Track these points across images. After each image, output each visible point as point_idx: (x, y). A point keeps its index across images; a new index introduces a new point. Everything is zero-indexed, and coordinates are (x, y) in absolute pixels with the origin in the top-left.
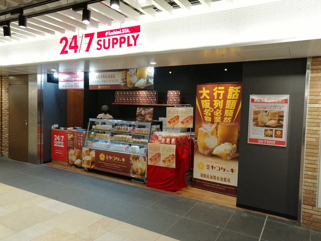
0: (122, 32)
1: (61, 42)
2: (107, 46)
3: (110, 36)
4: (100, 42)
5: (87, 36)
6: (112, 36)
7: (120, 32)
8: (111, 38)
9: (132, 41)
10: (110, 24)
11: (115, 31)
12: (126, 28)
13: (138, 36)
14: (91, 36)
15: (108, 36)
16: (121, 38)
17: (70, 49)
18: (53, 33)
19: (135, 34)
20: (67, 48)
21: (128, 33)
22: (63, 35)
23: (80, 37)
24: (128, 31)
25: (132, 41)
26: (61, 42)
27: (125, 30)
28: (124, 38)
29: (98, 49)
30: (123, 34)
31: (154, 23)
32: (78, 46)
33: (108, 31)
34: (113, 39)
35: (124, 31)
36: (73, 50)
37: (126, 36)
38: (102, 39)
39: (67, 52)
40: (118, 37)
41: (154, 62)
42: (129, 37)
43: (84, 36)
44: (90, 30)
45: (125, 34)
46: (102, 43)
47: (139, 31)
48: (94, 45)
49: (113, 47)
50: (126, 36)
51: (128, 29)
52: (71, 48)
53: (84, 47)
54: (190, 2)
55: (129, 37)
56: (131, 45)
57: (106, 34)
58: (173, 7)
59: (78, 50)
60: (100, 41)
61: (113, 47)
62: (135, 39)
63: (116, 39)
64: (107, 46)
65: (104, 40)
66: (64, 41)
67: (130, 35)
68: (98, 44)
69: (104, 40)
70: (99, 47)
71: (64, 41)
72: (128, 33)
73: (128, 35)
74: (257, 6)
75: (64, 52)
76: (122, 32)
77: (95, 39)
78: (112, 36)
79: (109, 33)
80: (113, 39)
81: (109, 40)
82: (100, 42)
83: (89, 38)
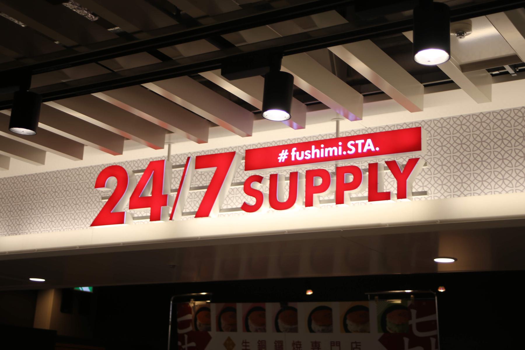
0: (345, 148)
1: (100, 183)
2: (284, 195)
3: (297, 162)
4: (256, 186)
5: (202, 161)
6: (305, 162)
7: (337, 151)
8: (302, 170)
9: (388, 182)
10: (117, 150)
11: (318, 147)
12: (365, 137)
13: (413, 163)
14: (221, 161)
15: (288, 162)
16: (340, 172)
17: (132, 206)
18: (74, 150)
19: (402, 159)
20: (124, 205)
21: (370, 153)
22: (107, 159)
23: (174, 167)
24: (370, 145)
25: (388, 182)
26: (100, 183)
27: (360, 142)
28: (356, 171)
29: (246, 208)
30: (348, 157)
31: (445, 124)
32: (166, 196)
33: (289, 147)
34: (310, 175)
35: (356, 146)
36: (147, 211)
37: (363, 164)
38: (266, 173)
39: (120, 219)
40: (330, 167)
41: (437, 263)
42: (373, 168)
43: (192, 165)
44: (220, 142)
45: (357, 155)
46: (264, 187)
47: (418, 147)
48: (232, 194)
49: (309, 203)
50: (363, 164)
51: (369, 141)
52: (137, 202)
53: (192, 199)
54: (421, 83)
55: (373, 168)
56: (387, 196)
57: (283, 156)
58: (307, 105)
59: (167, 210)
60: (259, 179)
61: (309, 203)
62: (402, 175)
63: (324, 174)
64: (284, 195)
65: (274, 178)
66: (112, 181)
67: (382, 160)
68: (249, 191)
69: (274, 178)
70: (252, 201)
71: (112, 181)
72: (370, 153)
73: (372, 160)
74: (475, 117)
75: (109, 216)
76: (345, 148)
77: (237, 172)
78: (305, 162)
79: (293, 153)
80: (310, 175)
81: (294, 177)
82: (256, 186)
83: (208, 173)
